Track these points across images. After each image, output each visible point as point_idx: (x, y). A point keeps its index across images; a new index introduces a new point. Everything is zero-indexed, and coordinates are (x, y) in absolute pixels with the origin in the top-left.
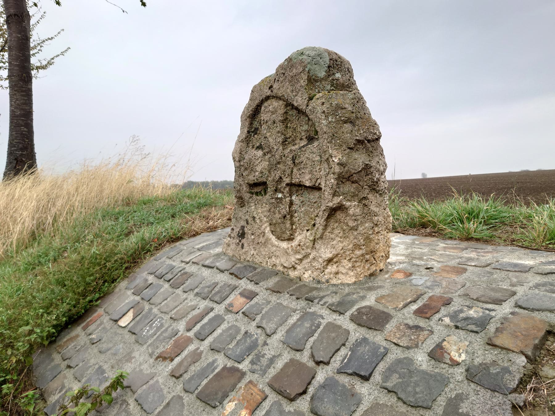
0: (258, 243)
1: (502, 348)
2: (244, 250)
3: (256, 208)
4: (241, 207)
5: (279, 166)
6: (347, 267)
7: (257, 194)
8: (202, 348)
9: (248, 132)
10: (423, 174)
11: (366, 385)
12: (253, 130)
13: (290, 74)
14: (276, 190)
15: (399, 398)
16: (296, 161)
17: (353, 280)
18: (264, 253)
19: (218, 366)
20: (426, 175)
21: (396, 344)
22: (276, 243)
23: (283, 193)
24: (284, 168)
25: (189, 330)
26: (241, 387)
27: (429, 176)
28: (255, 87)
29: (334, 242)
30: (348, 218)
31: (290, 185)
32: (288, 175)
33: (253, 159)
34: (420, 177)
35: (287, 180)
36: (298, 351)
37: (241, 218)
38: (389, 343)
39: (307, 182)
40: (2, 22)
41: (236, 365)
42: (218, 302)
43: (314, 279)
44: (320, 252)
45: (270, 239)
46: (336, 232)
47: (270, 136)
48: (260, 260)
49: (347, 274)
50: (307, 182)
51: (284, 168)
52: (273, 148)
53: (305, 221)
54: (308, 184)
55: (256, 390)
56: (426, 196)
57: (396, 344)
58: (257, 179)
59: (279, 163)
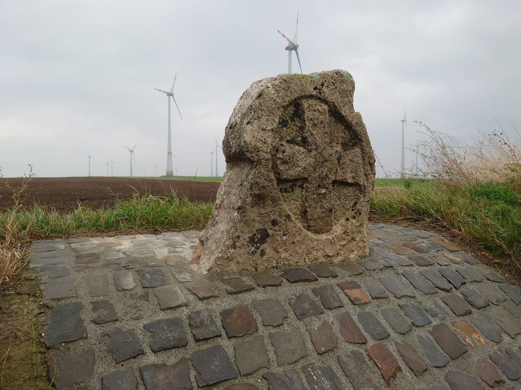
0: (293, 243)
2: (265, 257)
4: (253, 207)
5: (325, 164)
7: (286, 191)
13: (342, 87)
14: (319, 186)
16: (341, 162)
18: (300, 251)
22: (315, 237)
23: (327, 188)
24: (331, 166)
26: (454, 330)
31: (335, 182)
35: (332, 177)
37: (254, 220)
39: (349, 180)
40: (423, 386)
43: (359, 257)
45: (308, 235)
48: (296, 260)
50: (349, 180)
51: (331, 166)
52: (320, 146)
53: (341, 213)
54: (350, 181)
56: (500, 183)
59: (326, 161)
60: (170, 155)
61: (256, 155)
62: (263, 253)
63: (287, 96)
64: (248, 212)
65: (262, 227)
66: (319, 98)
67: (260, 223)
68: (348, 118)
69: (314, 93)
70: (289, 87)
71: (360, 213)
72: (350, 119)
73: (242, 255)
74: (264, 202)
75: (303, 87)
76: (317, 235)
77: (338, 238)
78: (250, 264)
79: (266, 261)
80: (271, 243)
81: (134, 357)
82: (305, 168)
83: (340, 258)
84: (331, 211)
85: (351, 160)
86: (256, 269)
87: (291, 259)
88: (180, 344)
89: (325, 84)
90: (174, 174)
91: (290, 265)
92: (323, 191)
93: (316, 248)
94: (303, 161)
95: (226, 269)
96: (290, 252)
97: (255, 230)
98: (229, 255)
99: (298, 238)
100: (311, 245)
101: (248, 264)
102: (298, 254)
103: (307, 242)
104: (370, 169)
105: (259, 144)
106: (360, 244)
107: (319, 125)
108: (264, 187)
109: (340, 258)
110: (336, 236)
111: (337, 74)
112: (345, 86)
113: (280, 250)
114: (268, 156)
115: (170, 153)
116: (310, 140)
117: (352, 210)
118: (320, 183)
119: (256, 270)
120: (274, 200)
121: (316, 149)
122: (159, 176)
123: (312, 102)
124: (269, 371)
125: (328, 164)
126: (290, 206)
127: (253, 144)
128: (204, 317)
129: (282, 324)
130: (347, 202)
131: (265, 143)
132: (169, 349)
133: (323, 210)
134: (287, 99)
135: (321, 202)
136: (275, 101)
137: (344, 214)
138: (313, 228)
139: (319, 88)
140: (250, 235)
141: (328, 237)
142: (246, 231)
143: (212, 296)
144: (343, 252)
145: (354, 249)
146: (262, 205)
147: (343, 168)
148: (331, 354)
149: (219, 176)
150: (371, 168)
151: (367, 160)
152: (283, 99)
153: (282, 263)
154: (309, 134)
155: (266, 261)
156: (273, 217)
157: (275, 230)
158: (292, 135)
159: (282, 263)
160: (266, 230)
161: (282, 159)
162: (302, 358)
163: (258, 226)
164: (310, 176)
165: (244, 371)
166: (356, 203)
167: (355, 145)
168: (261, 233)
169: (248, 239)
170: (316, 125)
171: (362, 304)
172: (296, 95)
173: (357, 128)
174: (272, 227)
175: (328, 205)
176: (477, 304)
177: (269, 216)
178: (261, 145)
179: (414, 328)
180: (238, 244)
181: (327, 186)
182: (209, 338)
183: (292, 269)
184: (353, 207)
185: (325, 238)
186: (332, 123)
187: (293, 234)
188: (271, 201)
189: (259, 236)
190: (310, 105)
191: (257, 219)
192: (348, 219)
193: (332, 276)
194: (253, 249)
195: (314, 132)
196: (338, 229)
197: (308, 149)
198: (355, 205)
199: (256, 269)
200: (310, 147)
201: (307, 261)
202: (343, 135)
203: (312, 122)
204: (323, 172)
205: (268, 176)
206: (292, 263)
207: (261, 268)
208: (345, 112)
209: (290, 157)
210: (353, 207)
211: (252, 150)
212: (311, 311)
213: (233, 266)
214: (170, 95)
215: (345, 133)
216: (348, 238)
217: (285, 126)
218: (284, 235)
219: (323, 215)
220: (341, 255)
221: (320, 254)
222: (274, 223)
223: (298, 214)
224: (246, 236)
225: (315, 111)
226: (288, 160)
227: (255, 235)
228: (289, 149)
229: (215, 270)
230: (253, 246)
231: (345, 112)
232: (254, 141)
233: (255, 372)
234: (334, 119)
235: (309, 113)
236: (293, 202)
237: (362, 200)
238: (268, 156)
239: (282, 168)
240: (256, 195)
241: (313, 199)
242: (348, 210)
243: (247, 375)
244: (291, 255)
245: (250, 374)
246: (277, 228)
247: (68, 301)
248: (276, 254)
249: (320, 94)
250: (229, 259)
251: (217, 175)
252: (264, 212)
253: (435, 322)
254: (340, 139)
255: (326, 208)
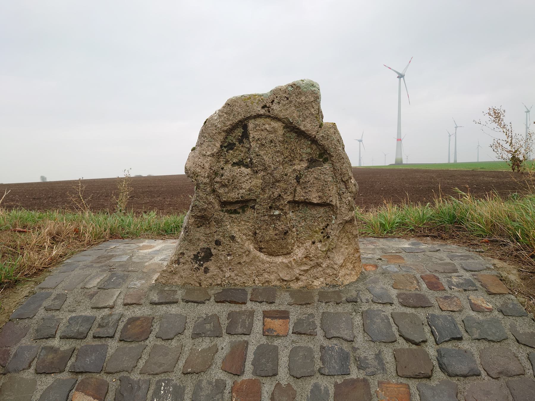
0: (240, 263)
1: (500, 294)
2: (208, 275)
3: (231, 227)
4: (198, 227)
5: (278, 184)
6: (350, 269)
8: (284, 383)
9: (221, 146)
10: (42, 177)
11: (463, 342)
12: (226, 144)
14: (271, 208)
15: (489, 341)
17: (356, 278)
19: (326, 388)
20: (46, 179)
21: (451, 311)
22: (268, 259)
24: (285, 186)
25: (239, 373)
26: (376, 392)
27: (48, 180)
28: (231, 100)
29: (342, 250)
30: (353, 228)
32: (291, 193)
33: (238, 175)
34: (39, 180)
35: (290, 198)
36: (393, 342)
37: (199, 239)
38: (448, 312)
39: (314, 200)
41: (347, 377)
42: (246, 333)
43: (327, 285)
44: (334, 259)
46: (344, 240)
47: (265, 154)
48: (242, 280)
49: (351, 274)
51: (285, 186)
52: (270, 167)
54: (315, 201)
55: (394, 386)
57: (451, 311)
58: (242, 197)
60: (399, 142)
61: (195, 179)
62: (206, 271)
63: (228, 120)
64: (192, 232)
65: (206, 246)
66: (269, 117)
67: (206, 242)
68: (309, 132)
69: (262, 112)
70: (232, 110)
71: (328, 237)
72: (314, 133)
73: (185, 270)
74: (209, 223)
75: (247, 108)
76: (271, 257)
77: (296, 262)
78: (194, 279)
79: (210, 278)
80: (215, 261)
81: (47, 338)
82: (250, 190)
83: (300, 283)
84: (286, 233)
85: (316, 178)
86: (200, 284)
87: (237, 279)
88: (79, 337)
89: (276, 101)
90: (404, 162)
91: (235, 285)
92: (277, 212)
93: (268, 270)
94: (247, 182)
95: (170, 281)
96: (236, 272)
97: (199, 249)
98: (172, 269)
99: (245, 258)
100: (262, 267)
101: (192, 279)
102: (246, 274)
103: (257, 263)
104: (344, 186)
105: (198, 170)
106: (329, 271)
107: (268, 145)
108: (205, 210)
109: (300, 283)
110: (294, 259)
111: (292, 87)
112: (303, 98)
113: (224, 269)
114: (207, 180)
115: (399, 140)
116: (255, 161)
117: (322, 233)
118: (272, 205)
119: (200, 286)
120: (219, 222)
121: (265, 169)
122: (387, 164)
123: (259, 121)
124: (129, 375)
125: (281, 184)
126: (238, 228)
127: (192, 169)
128: (112, 319)
129: (149, 337)
130: (316, 224)
131: (203, 168)
132: (70, 338)
133: (277, 232)
134: (228, 123)
135: (274, 224)
136: (216, 126)
137: (311, 236)
138: (265, 250)
139: (268, 105)
140: (195, 253)
141: (284, 260)
142: (192, 249)
143: (135, 304)
144: (306, 278)
145: (318, 275)
146: (208, 226)
147: (304, 188)
148: (195, 376)
149: (459, 161)
150: (346, 186)
151: (339, 177)
152: (224, 123)
153: (227, 281)
154: (254, 155)
155: (210, 278)
156: (216, 237)
157: (219, 250)
158: (239, 158)
159: (227, 281)
160: (209, 249)
161: (221, 182)
162: (165, 372)
163: (203, 245)
164: (258, 197)
165: (108, 369)
166: (328, 225)
167: (326, 160)
168: (205, 252)
169: (192, 257)
170: (263, 145)
171: (273, 336)
172: (240, 118)
173: (324, 142)
174: (216, 246)
175: (283, 227)
176: (450, 370)
177: (213, 236)
178: (200, 171)
179: (318, 375)
180: (182, 260)
181: (281, 207)
182: (102, 337)
183: (238, 290)
184: (324, 229)
185: (280, 260)
186: (292, 140)
187: (239, 255)
188: (215, 222)
189: (203, 254)
190: (257, 125)
191: (202, 238)
192: (314, 243)
193: (267, 302)
194: (196, 266)
195: (262, 153)
196: (299, 253)
197: (254, 170)
198: (326, 227)
199: (200, 284)
200: (256, 169)
201: (257, 282)
202: (309, 150)
203: (259, 142)
204: (273, 193)
205: (207, 199)
206: (237, 283)
207: (204, 284)
208: (305, 126)
209: (229, 180)
210: (324, 229)
211: (191, 175)
212: (209, 333)
213: (176, 279)
214: (401, 76)
215: (312, 149)
216: (311, 263)
217: (232, 149)
218: (228, 255)
219: (276, 237)
220: (302, 281)
221: (272, 277)
222: (218, 243)
223: (249, 235)
224: (192, 254)
225: (262, 130)
226: (227, 183)
227: (199, 253)
228: (229, 171)
229: (160, 280)
230: (197, 263)
231: (305, 126)
232: (193, 167)
233: (116, 372)
234: (294, 135)
235: (256, 133)
236: (243, 223)
237: (333, 222)
238: (207, 180)
239: (221, 191)
240: (198, 216)
241: (264, 221)
242: (316, 232)
243: (109, 373)
244: (236, 275)
245: (112, 373)
246: (220, 248)
247: (47, 290)
248: (221, 273)
249: (269, 112)
250: (174, 273)
251: (455, 161)
252: (208, 232)
253: (355, 374)
254: (304, 156)
255: (281, 230)
